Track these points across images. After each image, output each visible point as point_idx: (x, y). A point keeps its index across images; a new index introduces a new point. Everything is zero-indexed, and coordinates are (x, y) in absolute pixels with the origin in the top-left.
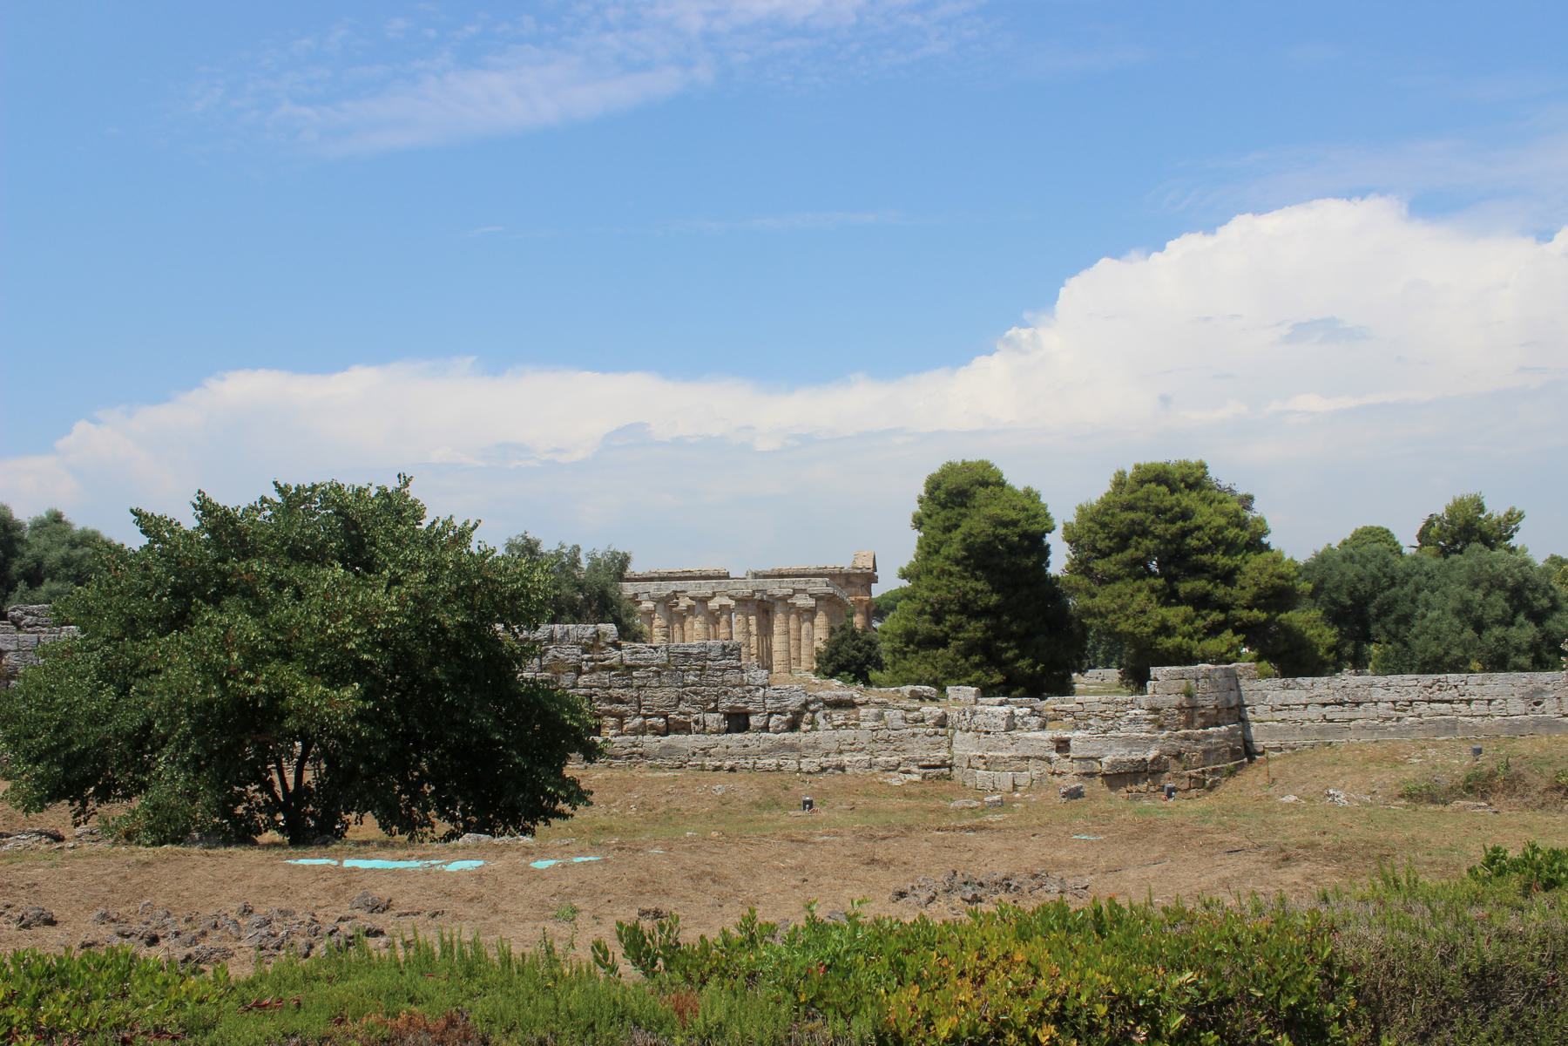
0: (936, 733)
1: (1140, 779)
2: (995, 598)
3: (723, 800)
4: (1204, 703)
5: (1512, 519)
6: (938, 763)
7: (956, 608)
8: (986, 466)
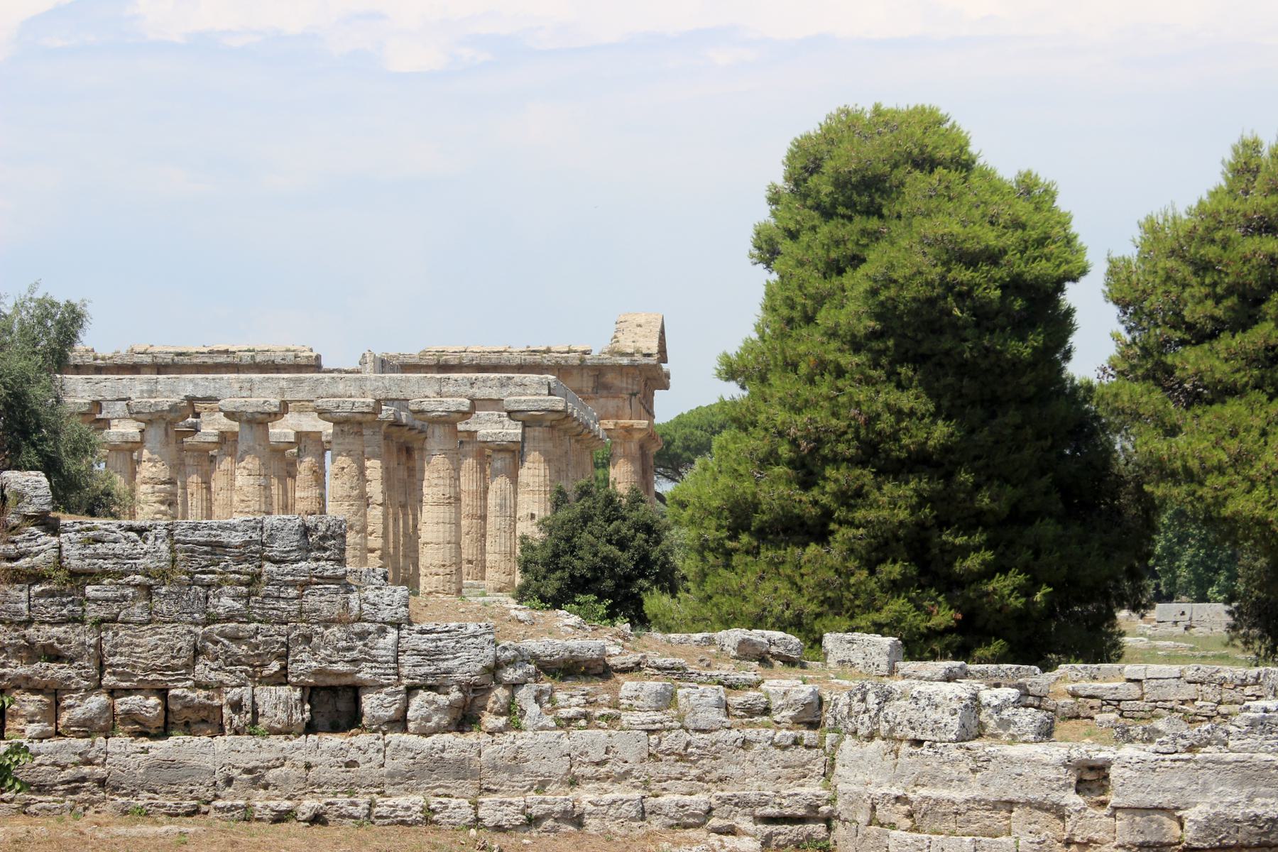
0: (797, 742)
2: (941, 431)
8: (931, 121)
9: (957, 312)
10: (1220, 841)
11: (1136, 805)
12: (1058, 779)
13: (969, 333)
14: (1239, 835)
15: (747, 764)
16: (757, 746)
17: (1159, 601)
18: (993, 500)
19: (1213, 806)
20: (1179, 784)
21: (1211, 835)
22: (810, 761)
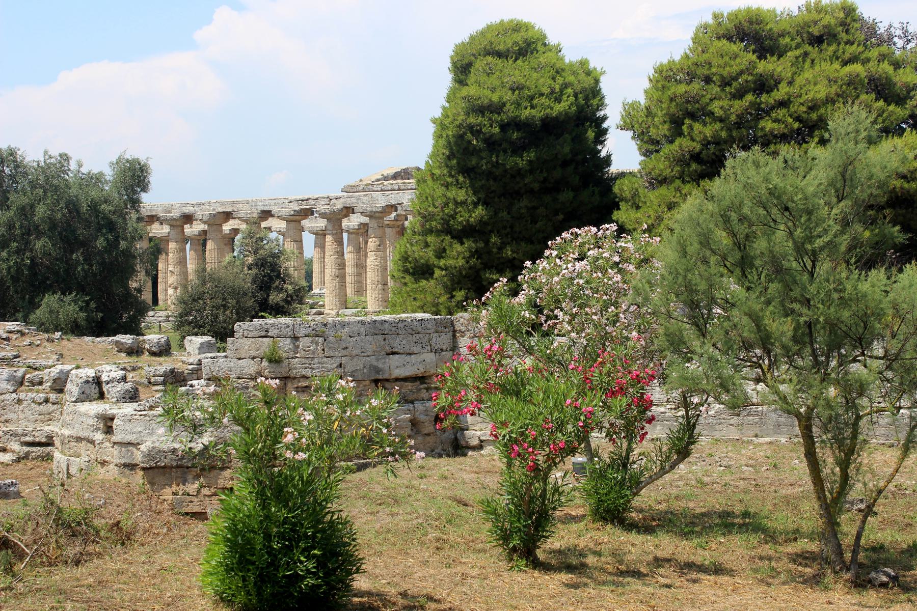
0: (47, 401)
1: (190, 477)
2: (480, 211)
3: (900, 488)
4: (308, 372)
5: (434, 121)
6: (44, 440)
7: (439, 227)
8: (517, 27)
9: (475, 142)
10: (156, 463)
11: (120, 441)
12: (93, 425)
13: (484, 154)
14: (166, 460)
15: (19, 413)
16: (25, 403)
17: (241, 319)
18: (513, 252)
19: (153, 442)
20: (140, 429)
21: (150, 460)
22: (53, 411)
